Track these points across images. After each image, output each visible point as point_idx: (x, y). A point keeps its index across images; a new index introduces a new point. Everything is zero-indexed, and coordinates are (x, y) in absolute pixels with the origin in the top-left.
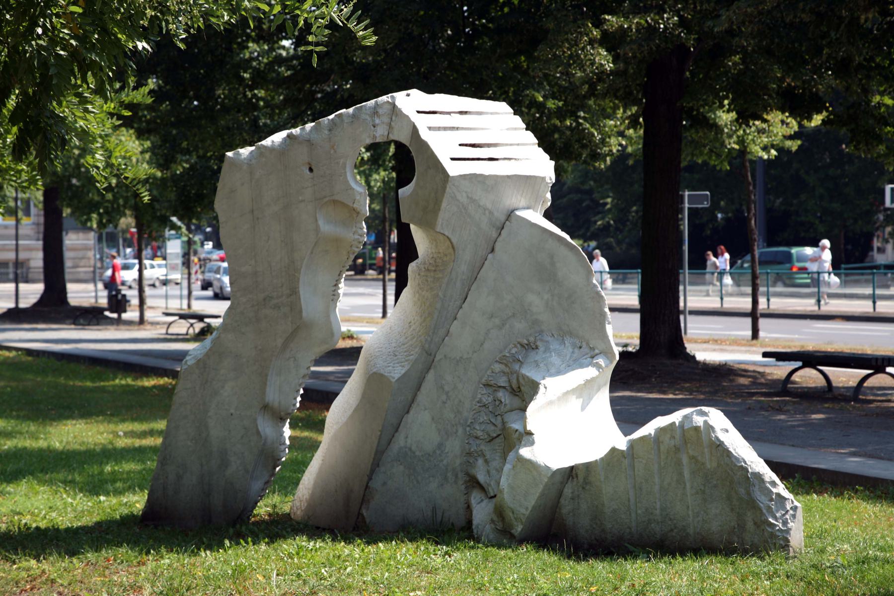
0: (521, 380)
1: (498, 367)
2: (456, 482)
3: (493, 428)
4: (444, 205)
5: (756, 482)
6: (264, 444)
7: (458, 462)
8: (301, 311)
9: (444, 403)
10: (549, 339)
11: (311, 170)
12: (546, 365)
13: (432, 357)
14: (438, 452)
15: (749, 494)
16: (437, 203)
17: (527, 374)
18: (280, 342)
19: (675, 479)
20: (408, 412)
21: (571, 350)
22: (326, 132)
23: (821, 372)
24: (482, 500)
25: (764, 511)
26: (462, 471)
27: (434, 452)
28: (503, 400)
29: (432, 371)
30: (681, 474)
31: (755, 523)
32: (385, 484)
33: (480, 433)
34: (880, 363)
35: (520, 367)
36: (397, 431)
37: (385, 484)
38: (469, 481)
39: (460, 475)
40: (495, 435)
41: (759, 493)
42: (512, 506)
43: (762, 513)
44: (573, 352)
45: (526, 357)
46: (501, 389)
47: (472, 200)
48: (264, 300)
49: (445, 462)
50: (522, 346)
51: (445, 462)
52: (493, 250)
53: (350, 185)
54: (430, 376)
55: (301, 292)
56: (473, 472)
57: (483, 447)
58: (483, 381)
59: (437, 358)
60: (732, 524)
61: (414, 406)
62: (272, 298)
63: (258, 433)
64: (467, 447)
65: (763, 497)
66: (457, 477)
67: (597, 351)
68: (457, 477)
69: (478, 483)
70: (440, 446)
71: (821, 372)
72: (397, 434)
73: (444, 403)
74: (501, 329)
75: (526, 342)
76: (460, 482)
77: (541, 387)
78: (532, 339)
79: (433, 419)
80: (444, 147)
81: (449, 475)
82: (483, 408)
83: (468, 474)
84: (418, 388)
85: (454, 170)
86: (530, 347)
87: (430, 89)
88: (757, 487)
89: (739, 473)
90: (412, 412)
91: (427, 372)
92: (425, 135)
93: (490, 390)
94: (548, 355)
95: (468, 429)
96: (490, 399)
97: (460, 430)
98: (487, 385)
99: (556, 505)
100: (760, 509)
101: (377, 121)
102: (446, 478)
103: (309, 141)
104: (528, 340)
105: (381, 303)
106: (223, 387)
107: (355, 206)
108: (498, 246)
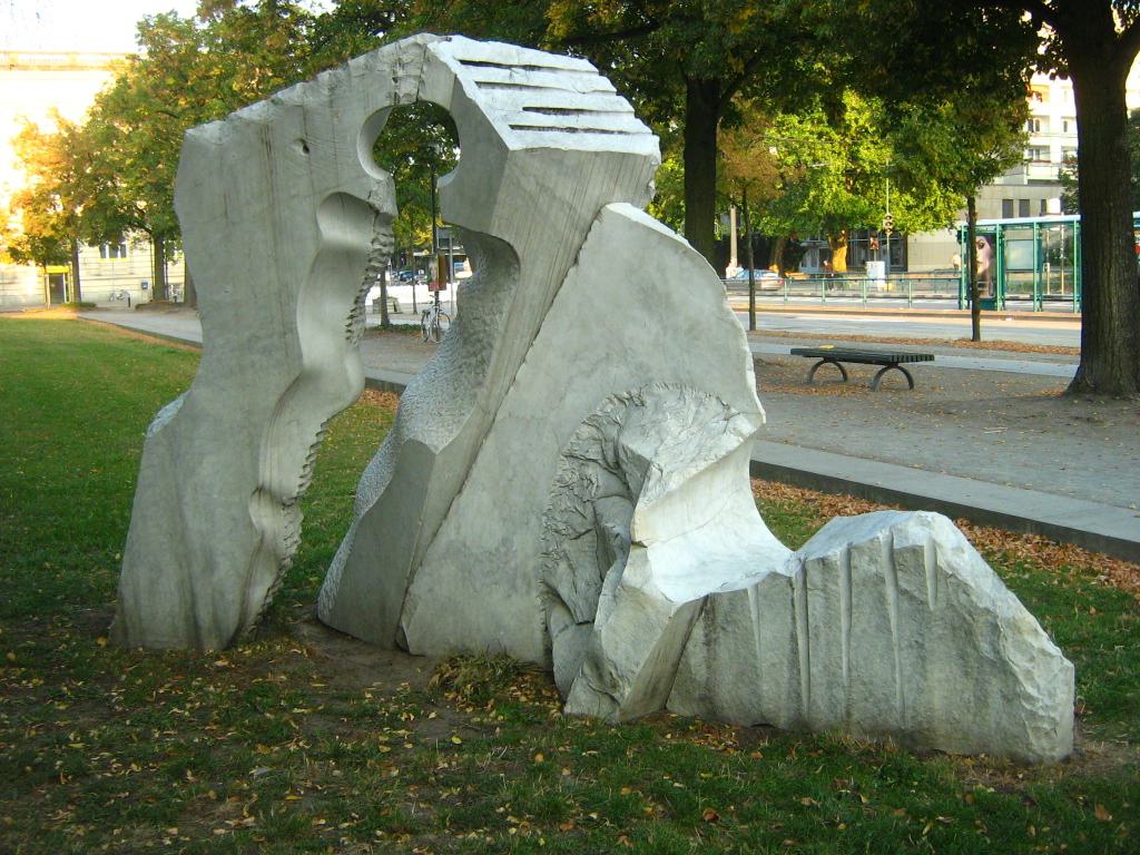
0: (622, 455)
1: (586, 431)
2: (528, 593)
3: (580, 519)
4: (501, 196)
5: (1009, 633)
6: (262, 541)
7: (531, 564)
8: (300, 356)
9: (510, 480)
10: (662, 391)
11: (306, 149)
12: (658, 433)
13: (491, 418)
14: (502, 550)
15: (997, 652)
16: (492, 192)
17: (633, 447)
18: (273, 399)
19: (873, 624)
20: (460, 492)
21: (694, 408)
22: (326, 92)
23: (839, 365)
24: (567, 627)
25: (1021, 678)
26: (536, 577)
27: (497, 549)
28: (594, 480)
29: (492, 435)
30: (886, 618)
31: (1004, 697)
32: (431, 590)
33: (561, 526)
34: (895, 360)
35: (620, 432)
36: (445, 517)
37: (431, 590)
38: (548, 593)
39: (534, 583)
40: (583, 531)
41: (1012, 650)
42: (613, 657)
43: (1017, 681)
44: (697, 412)
45: (628, 416)
46: (591, 463)
47: (543, 188)
48: (249, 340)
49: (513, 564)
50: (621, 401)
51: (513, 564)
52: (576, 261)
53: (362, 170)
54: (489, 444)
55: (299, 330)
56: (554, 582)
57: (566, 546)
58: (565, 450)
59: (499, 417)
60: (966, 696)
61: (468, 484)
62: (258, 338)
63: (251, 525)
64: (543, 544)
65: (1019, 656)
66: (529, 585)
67: (733, 410)
68: (529, 585)
69: (559, 596)
70: (505, 541)
71: (839, 365)
72: (445, 524)
73: (510, 480)
74: (589, 376)
75: (626, 395)
76: (534, 594)
77: (654, 469)
78: (635, 392)
79: (494, 503)
80: (497, 107)
81: (519, 582)
82: (565, 490)
83: (547, 585)
84: (474, 457)
85: (514, 142)
86: (634, 402)
87: (477, 34)
88: (1010, 640)
89: (982, 619)
90: (465, 492)
91: (486, 436)
92: (471, 91)
93: (576, 464)
94: (660, 416)
95: (544, 518)
96: (576, 478)
97: (534, 521)
98: (571, 456)
99: (678, 666)
100: (1013, 674)
101: (400, 73)
102: (514, 587)
103: (301, 106)
104: (629, 393)
105: (1012, 187)
106: (201, 463)
107: (371, 200)
108: (583, 256)
